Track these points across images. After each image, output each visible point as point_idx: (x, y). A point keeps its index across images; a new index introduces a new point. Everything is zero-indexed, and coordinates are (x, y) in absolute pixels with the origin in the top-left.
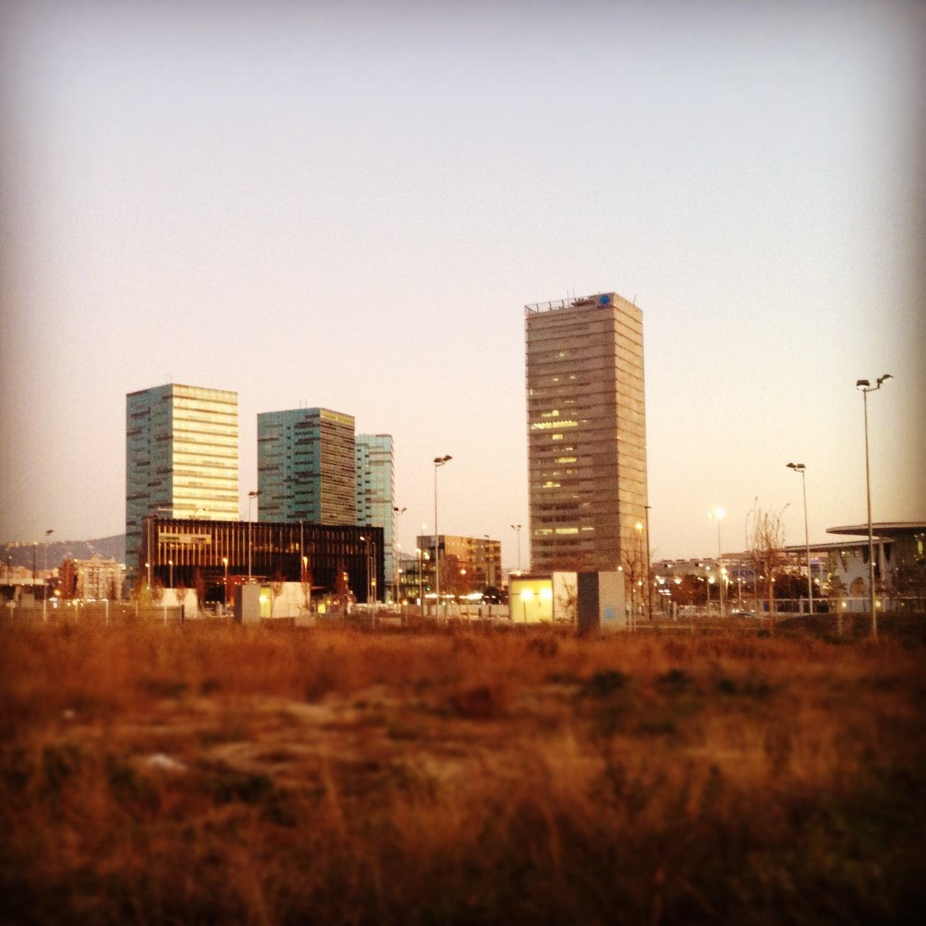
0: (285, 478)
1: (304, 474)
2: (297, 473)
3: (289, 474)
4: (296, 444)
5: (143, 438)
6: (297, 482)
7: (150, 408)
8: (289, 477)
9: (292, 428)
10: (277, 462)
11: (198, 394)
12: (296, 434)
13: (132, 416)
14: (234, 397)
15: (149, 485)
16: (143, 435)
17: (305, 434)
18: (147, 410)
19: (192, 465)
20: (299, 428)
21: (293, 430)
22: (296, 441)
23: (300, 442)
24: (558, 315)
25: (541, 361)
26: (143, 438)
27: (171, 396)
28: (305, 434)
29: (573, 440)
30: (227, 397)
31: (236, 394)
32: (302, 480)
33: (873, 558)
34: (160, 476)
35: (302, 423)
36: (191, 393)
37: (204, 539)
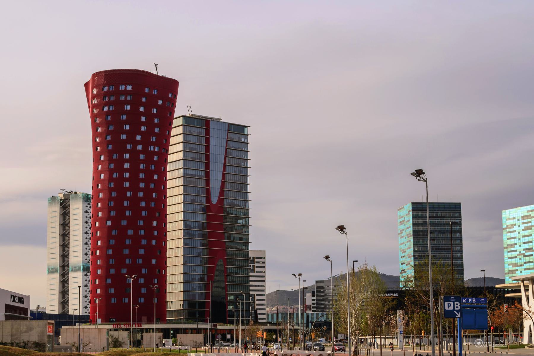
2: (524, 250)
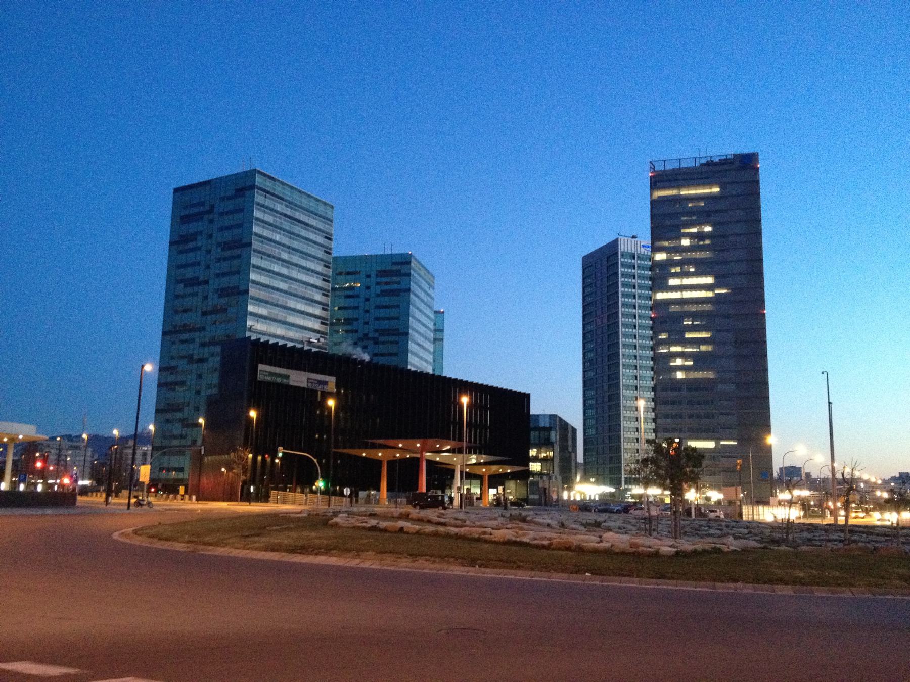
0: (360, 335)
1: (384, 332)
2: (376, 331)
3: (366, 332)
4: (378, 295)
5: (199, 248)
6: (376, 342)
7: (213, 206)
8: (366, 335)
9: (373, 275)
10: (181, 400)
11: (287, 194)
12: (378, 284)
13: (182, 218)
14: (329, 211)
15: (204, 314)
16: (199, 244)
17: (387, 283)
18: (207, 208)
19: (267, 286)
20: (381, 277)
21: (373, 279)
22: (379, 292)
23: (384, 293)
24: (684, 180)
25: (668, 223)
26: (199, 248)
27: (253, 187)
28: (387, 283)
29: (711, 315)
30: (321, 209)
31: (332, 207)
32: (382, 339)
33: (259, 464)
34: (223, 301)
35: (385, 271)
36: (278, 190)
37: (326, 383)
